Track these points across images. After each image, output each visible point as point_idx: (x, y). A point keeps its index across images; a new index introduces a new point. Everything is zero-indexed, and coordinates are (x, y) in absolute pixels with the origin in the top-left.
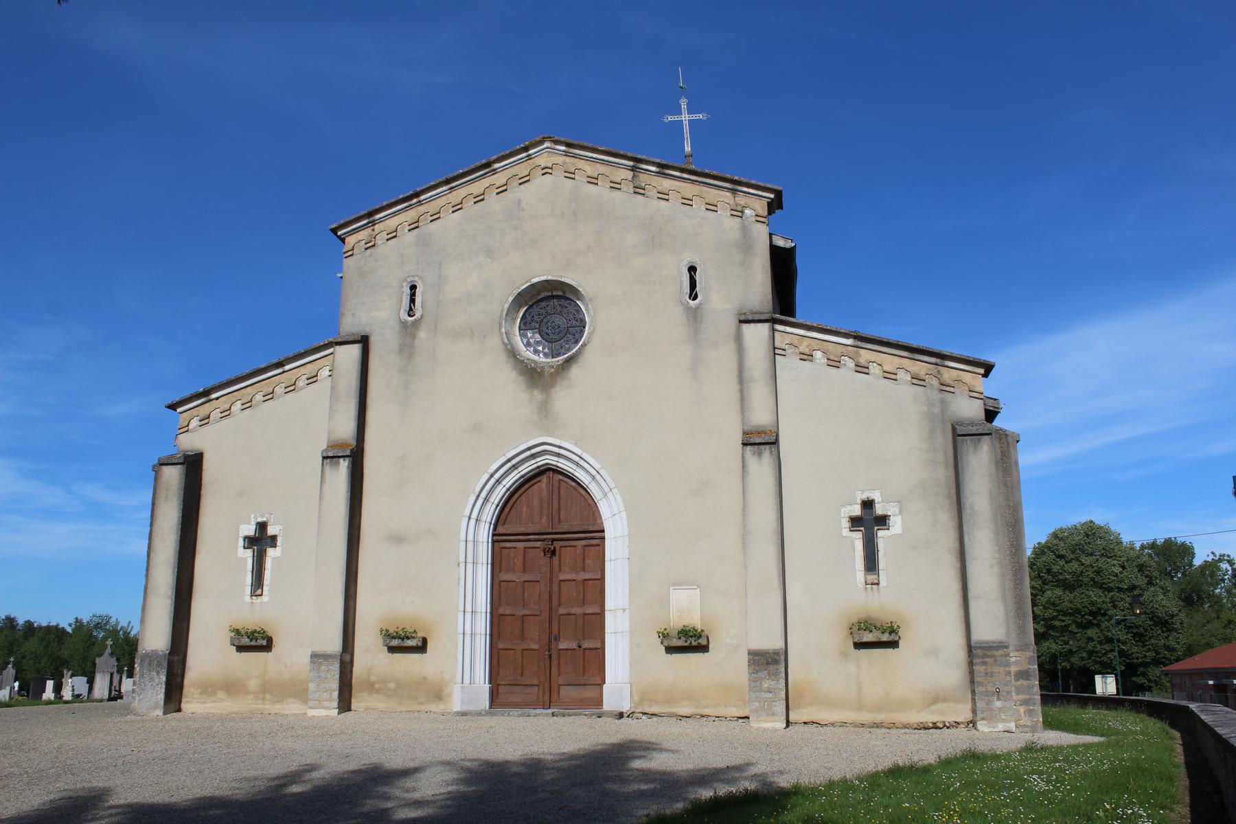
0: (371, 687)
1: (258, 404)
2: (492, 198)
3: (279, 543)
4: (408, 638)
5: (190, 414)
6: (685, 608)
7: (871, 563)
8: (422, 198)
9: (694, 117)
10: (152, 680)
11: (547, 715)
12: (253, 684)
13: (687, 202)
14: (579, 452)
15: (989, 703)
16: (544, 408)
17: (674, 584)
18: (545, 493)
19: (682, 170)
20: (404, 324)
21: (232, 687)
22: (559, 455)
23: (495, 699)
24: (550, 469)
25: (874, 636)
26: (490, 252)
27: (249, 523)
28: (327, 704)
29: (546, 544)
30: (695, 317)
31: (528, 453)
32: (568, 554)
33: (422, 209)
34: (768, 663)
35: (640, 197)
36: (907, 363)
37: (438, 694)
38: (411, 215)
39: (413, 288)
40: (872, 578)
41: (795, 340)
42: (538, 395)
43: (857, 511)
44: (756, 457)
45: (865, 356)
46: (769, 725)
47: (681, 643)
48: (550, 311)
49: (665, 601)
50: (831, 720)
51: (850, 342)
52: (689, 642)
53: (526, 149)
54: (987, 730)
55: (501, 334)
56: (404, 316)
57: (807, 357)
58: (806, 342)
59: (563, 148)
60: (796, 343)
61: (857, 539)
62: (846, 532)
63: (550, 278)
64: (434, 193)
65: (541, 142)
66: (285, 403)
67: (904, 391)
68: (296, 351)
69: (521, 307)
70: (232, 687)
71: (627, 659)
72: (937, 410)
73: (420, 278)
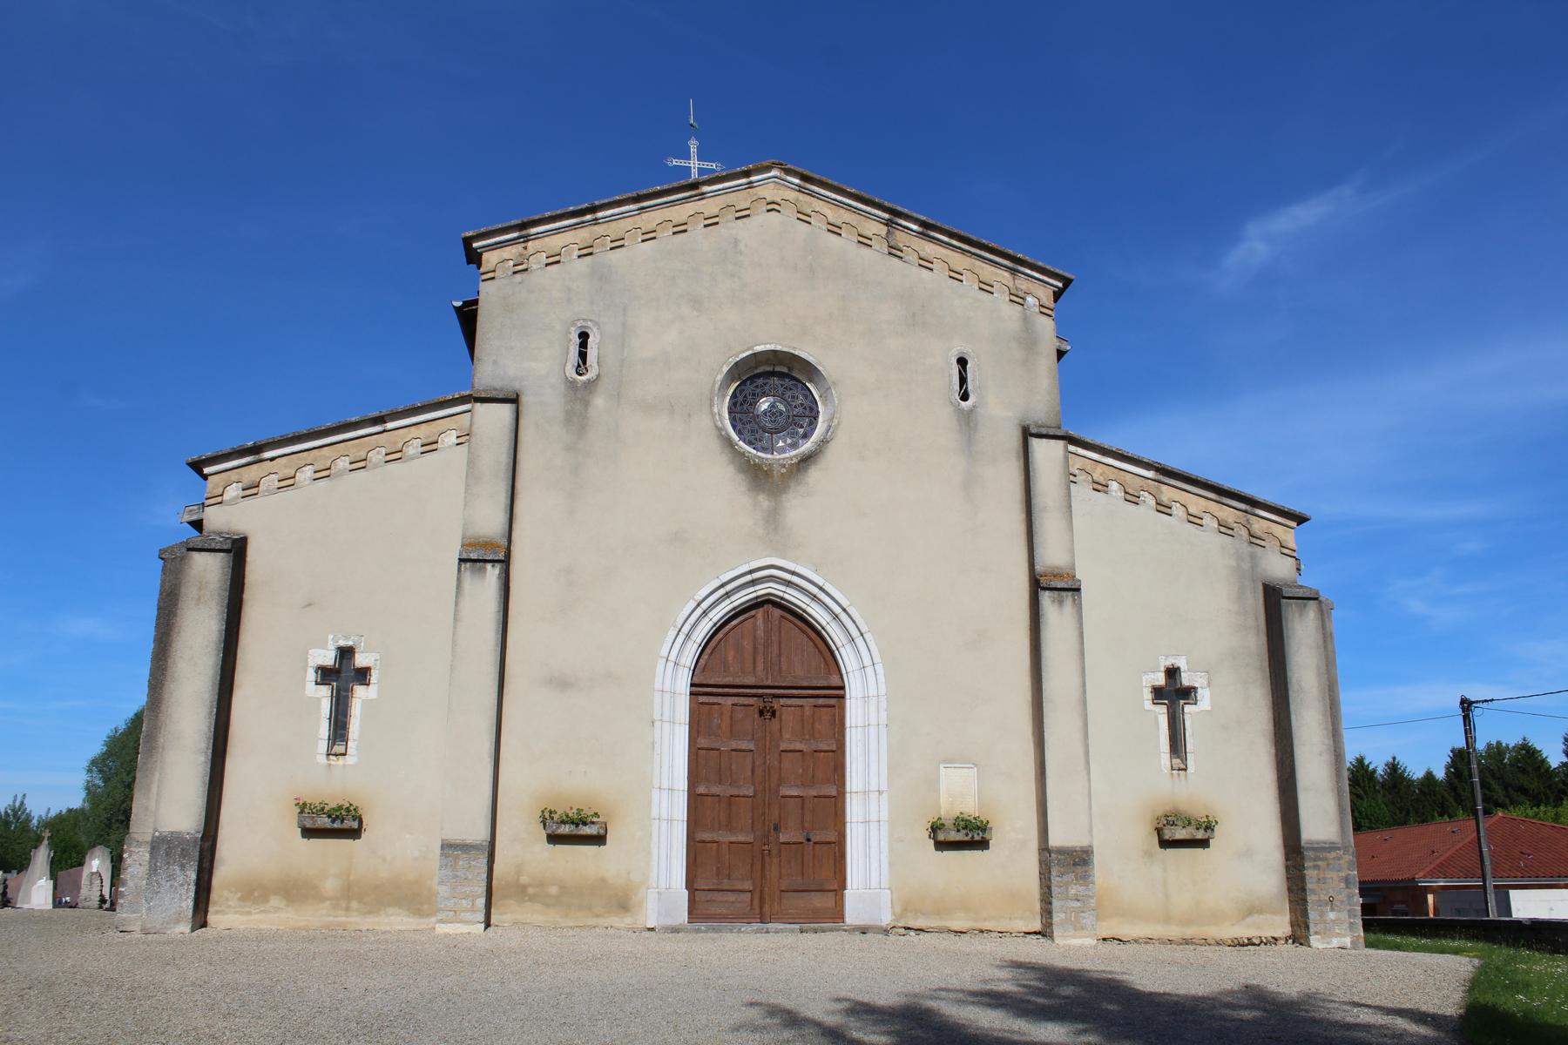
0: (521, 892)
1: (340, 474)
2: (697, 230)
3: (373, 679)
4: (585, 824)
5: (227, 480)
6: (959, 793)
7: (1177, 744)
8: (600, 214)
9: (682, 163)
10: (171, 877)
11: (792, 931)
12: (330, 886)
13: (955, 275)
14: (820, 582)
15: (1322, 914)
16: (773, 520)
17: (945, 761)
18: (760, 633)
19: (951, 235)
20: (572, 384)
21: (295, 890)
22: (789, 583)
23: (695, 912)
24: (769, 602)
25: (1182, 834)
26: (696, 303)
27: (324, 646)
28: (467, 916)
29: (768, 698)
30: (968, 422)
31: (748, 578)
32: (789, 712)
33: (599, 230)
34: (1075, 864)
35: (895, 260)
36: (1213, 507)
37: (623, 902)
38: (583, 235)
39: (584, 337)
40: (1177, 762)
41: (1088, 465)
42: (764, 501)
43: (1160, 680)
44: (1056, 605)
45: (1168, 493)
46: (1076, 942)
47: (960, 837)
48: (772, 394)
49: (933, 783)
50: (1135, 936)
51: (1150, 474)
52: (966, 836)
53: (747, 174)
54: (1321, 946)
55: (713, 414)
56: (571, 372)
57: (1100, 487)
58: (1100, 469)
59: (797, 181)
60: (1088, 468)
61: (1161, 712)
62: (1148, 705)
63: (779, 348)
64: (616, 210)
65: (768, 169)
66: (382, 479)
67: (1209, 541)
68: (409, 405)
69: (733, 381)
70: (295, 890)
71: (878, 858)
72: (1246, 566)
73: (596, 324)
